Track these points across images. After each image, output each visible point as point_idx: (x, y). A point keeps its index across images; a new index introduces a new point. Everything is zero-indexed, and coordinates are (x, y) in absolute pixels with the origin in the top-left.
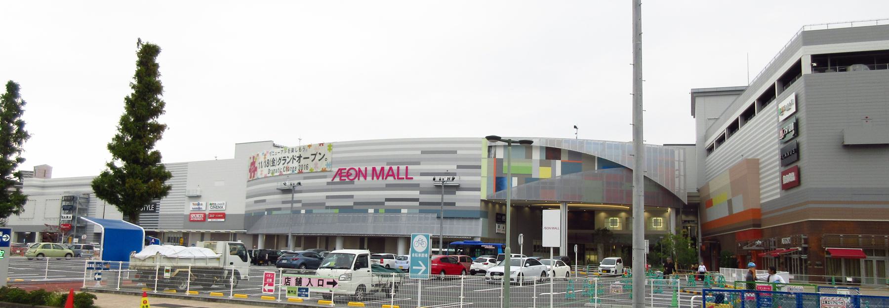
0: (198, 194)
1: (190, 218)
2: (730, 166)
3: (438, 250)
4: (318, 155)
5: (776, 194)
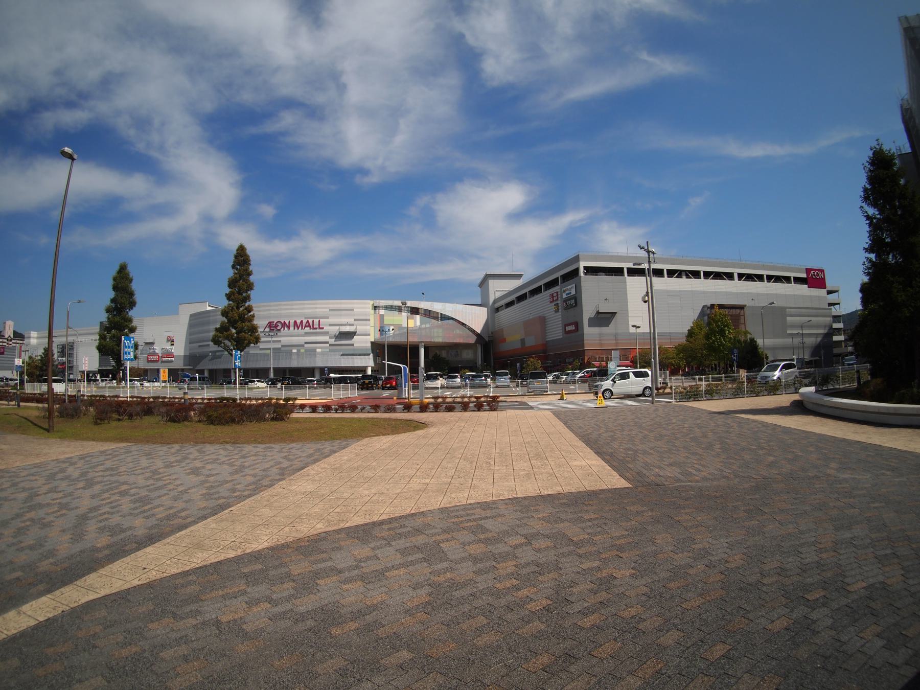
0: (151, 341)
1: (148, 359)
2: (306, 311)
3: (672, 401)
5: (560, 336)
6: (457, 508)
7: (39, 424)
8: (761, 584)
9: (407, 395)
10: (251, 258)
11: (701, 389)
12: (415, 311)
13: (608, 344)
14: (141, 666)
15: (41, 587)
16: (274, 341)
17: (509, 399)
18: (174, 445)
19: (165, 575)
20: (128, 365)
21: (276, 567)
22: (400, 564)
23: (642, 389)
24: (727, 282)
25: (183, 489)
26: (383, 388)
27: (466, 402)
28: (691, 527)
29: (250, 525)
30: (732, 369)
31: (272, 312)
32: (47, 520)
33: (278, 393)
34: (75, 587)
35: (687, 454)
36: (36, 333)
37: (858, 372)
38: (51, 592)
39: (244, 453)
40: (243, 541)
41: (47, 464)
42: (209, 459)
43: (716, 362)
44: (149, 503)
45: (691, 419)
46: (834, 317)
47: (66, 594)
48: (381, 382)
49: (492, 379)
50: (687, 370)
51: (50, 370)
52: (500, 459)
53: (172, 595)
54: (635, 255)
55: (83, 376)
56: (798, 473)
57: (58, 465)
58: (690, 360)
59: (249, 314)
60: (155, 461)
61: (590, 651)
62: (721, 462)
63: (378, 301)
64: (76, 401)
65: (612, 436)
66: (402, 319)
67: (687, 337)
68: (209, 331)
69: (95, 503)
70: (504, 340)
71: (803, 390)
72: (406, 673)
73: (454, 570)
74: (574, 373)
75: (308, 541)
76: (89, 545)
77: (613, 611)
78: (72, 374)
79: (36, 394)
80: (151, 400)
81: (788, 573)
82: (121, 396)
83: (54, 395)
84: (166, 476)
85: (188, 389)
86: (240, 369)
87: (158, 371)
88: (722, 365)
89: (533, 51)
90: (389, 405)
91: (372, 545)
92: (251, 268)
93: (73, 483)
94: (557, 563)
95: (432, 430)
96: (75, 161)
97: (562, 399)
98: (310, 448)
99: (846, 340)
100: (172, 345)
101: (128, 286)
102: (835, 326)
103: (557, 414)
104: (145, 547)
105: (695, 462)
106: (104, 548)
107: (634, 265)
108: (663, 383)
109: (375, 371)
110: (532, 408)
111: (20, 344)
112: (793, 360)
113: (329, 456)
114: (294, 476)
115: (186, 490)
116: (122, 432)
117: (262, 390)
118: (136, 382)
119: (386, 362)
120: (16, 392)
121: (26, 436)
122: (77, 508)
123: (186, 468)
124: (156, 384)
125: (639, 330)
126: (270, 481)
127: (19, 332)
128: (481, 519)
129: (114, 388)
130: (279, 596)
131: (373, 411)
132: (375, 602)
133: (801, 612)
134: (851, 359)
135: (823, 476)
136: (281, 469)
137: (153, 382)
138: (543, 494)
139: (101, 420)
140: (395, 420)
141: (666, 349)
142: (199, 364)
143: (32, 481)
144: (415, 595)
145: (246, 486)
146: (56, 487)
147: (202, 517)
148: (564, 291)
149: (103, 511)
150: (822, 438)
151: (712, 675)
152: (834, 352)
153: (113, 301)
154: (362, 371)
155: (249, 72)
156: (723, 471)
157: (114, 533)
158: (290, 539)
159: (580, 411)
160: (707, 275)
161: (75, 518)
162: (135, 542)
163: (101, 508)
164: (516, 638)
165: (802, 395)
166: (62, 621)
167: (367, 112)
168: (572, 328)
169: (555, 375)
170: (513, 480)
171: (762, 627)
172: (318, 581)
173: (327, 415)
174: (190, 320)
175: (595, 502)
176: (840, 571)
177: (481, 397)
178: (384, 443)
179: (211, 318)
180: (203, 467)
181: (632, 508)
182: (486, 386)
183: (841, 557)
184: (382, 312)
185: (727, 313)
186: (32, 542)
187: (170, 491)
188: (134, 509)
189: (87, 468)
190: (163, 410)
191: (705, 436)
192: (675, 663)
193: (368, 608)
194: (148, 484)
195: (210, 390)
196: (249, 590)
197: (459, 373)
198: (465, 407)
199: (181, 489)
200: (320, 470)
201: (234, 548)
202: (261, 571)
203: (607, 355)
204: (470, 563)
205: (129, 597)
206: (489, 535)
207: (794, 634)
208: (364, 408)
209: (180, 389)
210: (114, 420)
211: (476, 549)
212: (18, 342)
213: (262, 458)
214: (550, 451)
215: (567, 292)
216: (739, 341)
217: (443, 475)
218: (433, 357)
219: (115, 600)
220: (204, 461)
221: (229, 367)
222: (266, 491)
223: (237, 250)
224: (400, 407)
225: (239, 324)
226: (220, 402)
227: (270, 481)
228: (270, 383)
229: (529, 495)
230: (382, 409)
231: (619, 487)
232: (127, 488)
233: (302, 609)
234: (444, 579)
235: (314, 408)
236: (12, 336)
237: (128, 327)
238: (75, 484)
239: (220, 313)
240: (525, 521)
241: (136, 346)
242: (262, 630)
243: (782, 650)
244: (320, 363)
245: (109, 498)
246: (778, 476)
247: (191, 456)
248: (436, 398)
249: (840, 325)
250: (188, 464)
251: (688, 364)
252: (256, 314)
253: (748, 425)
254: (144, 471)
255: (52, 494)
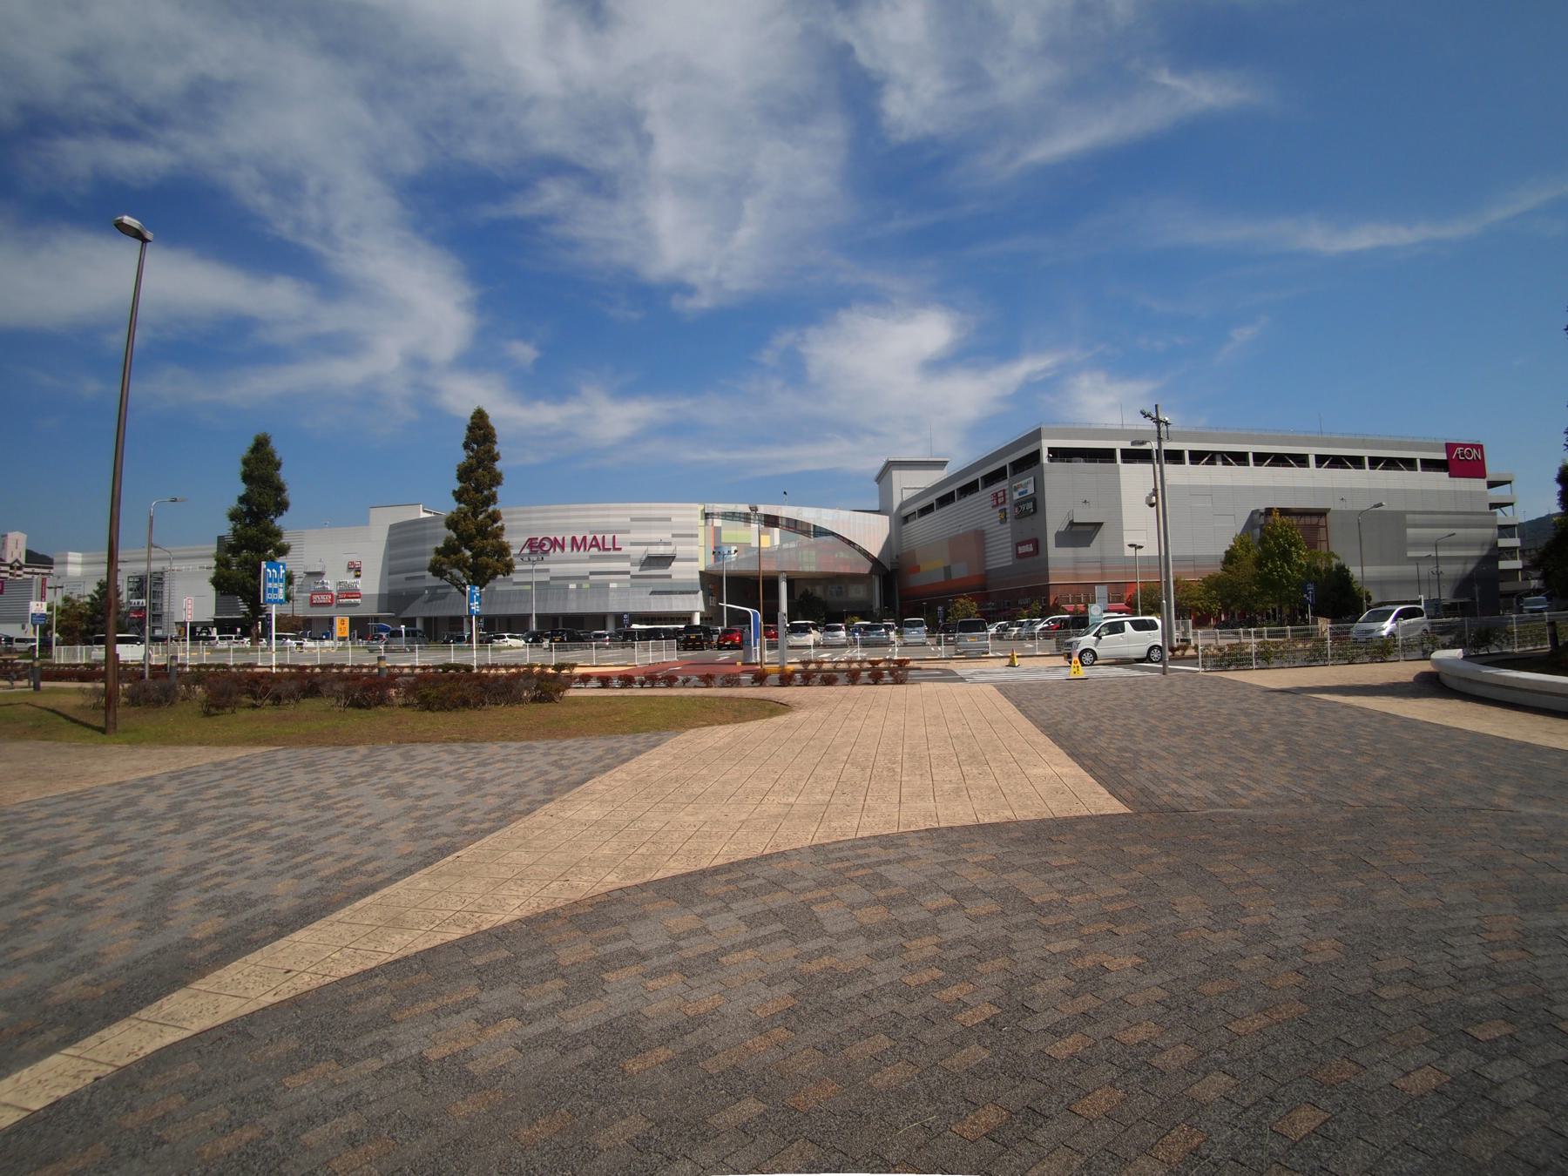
0: (318, 570)
6: (841, 845)
7: (84, 720)
8: (1375, 998)
9: (759, 659)
10: (496, 432)
11: (1249, 650)
12: (771, 521)
13: (1089, 575)
14: (256, 1168)
15: (51, 1036)
16: (538, 571)
17: (924, 665)
18: (358, 748)
19: (328, 979)
20: (274, 610)
21: (532, 954)
22: (745, 942)
23: (1145, 649)
24: (1296, 471)
25: (372, 822)
26: (720, 647)
27: (855, 670)
28: (1237, 886)
29: (490, 880)
30: (1303, 617)
31: (534, 522)
32: (87, 898)
33: (545, 657)
34: (135, 1022)
35: (1227, 761)
36: (80, 554)
37: (1552, 624)
38: (76, 1042)
39: (484, 757)
40: (477, 909)
41: (96, 792)
42: (421, 770)
43: (1276, 606)
44: (306, 851)
45: (1230, 701)
46: (1501, 527)
47: (111, 1042)
48: (715, 637)
49: (897, 632)
50: (1223, 618)
51: (112, 621)
52: (911, 764)
53: (338, 1017)
54: (1135, 428)
55: (183, 632)
56: (1436, 799)
57: (123, 792)
58: (1229, 601)
59: (495, 526)
60: (321, 775)
61: (1069, 1104)
62: (1288, 775)
63: (711, 505)
64: (167, 676)
65: (1096, 727)
66: (750, 534)
67: (1224, 563)
68: (424, 554)
69: (197, 856)
70: (916, 569)
71: (1439, 654)
72: (753, 1142)
73: (836, 951)
74: (1031, 623)
75: (591, 906)
76: (177, 937)
77: (1106, 1029)
78: (161, 628)
79: (79, 665)
80: (318, 670)
81: (1428, 982)
82: (259, 664)
83: (121, 665)
84: (340, 802)
85: (387, 650)
86: (479, 617)
87: (331, 621)
88: (1286, 611)
89: (970, 77)
90: (729, 675)
91: (699, 910)
92: (497, 448)
93: (154, 823)
94: (1007, 941)
95: (799, 716)
96: (148, 244)
97: (1012, 665)
98: (597, 746)
99: (1524, 569)
100: (358, 576)
101: (272, 475)
102: (1503, 543)
103: (1004, 689)
104: (293, 931)
105: (1241, 773)
106: (209, 939)
107: (1133, 444)
108: (1182, 640)
109: (706, 619)
110: (962, 679)
111: (43, 574)
112: (1419, 602)
113: (628, 759)
114: (570, 794)
115: (378, 824)
116: (258, 727)
117: (517, 651)
118: (289, 641)
119: (725, 604)
120: (31, 664)
121: (51, 743)
122: (157, 869)
123: (380, 786)
124: (327, 643)
125: (1140, 553)
126: (529, 804)
127: (40, 553)
128: (879, 864)
129: (244, 650)
130: (537, 1005)
131: (703, 684)
132: (702, 1010)
133: (1464, 1061)
134: (1540, 602)
135: (1486, 807)
136: (547, 782)
137: (321, 639)
138: (981, 822)
139: (218, 707)
140: (739, 699)
141: (1188, 584)
142: (405, 608)
143: (58, 826)
144: (769, 997)
145: (485, 813)
146: (114, 834)
147: (405, 870)
148: (1016, 489)
149: (213, 870)
150: (1505, 743)
151: (1298, 1168)
153: (242, 500)
154: (684, 619)
155: (479, 104)
156: (1291, 790)
157: (233, 909)
158: (560, 903)
159: (1042, 685)
160: (1260, 458)
161: (151, 888)
162: (275, 924)
163: (209, 866)
164: (941, 1076)
165: (1437, 662)
166: (89, 1100)
167: (689, 187)
168: (1029, 548)
169: (999, 626)
170: (932, 798)
171: (1385, 1082)
172: (605, 976)
173: (626, 692)
174: (389, 535)
175: (1068, 837)
176: (1540, 990)
177: (880, 662)
178: (721, 738)
179: (428, 532)
180: (411, 784)
181: (1132, 849)
182: (889, 644)
183: (1539, 962)
184: (718, 522)
185: (1295, 522)
186: (43, 946)
187: (347, 826)
188: (275, 863)
189: (185, 795)
190: (339, 687)
191: (1257, 729)
192: (1224, 1137)
193: (690, 1021)
194: (306, 816)
195: (424, 653)
196: (483, 997)
197: (843, 622)
198: (853, 678)
199: (367, 822)
200: (613, 783)
201: (460, 923)
202: (507, 961)
203: (1086, 593)
204: (862, 940)
205: (251, 1029)
206: (894, 891)
207: (1454, 1104)
208: (688, 680)
209: (371, 651)
210: (244, 708)
211: (872, 916)
212: (37, 570)
213: (515, 765)
214: (994, 751)
215: (1021, 490)
216: (1317, 571)
217: (818, 790)
218: (801, 596)
219: (221, 1039)
220: (411, 773)
221: (458, 613)
222: (520, 821)
223: (472, 418)
224: (747, 677)
225: (478, 542)
226: (444, 672)
227: (529, 804)
228: (530, 640)
229: (958, 823)
230: (718, 681)
231: (1109, 812)
232: (263, 826)
233: (575, 1027)
234: (818, 968)
235: (605, 681)
236: (23, 560)
237: (274, 546)
238: (157, 825)
239: (443, 523)
240: (952, 868)
241: (289, 579)
242: (501, 1071)
243: (1433, 1133)
244: (614, 605)
245: (226, 847)
246: (1396, 804)
247: (390, 766)
248: (805, 663)
249: (1515, 542)
250: (384, 778)
251: (1226, 609)
252: (507, 525)
253: (1335, 712)
254: (299, 795)
255: (105, 847)
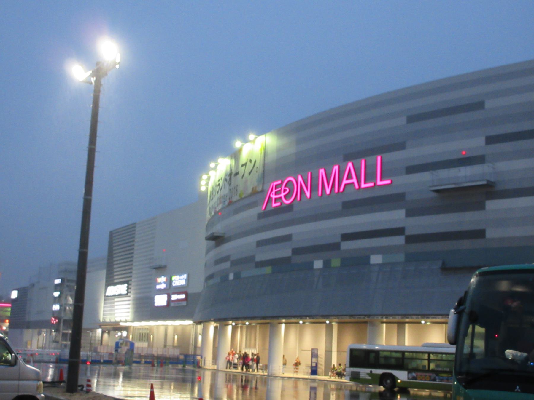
0: (163, 263)
4: (249, 163)
152: (53, 309)
